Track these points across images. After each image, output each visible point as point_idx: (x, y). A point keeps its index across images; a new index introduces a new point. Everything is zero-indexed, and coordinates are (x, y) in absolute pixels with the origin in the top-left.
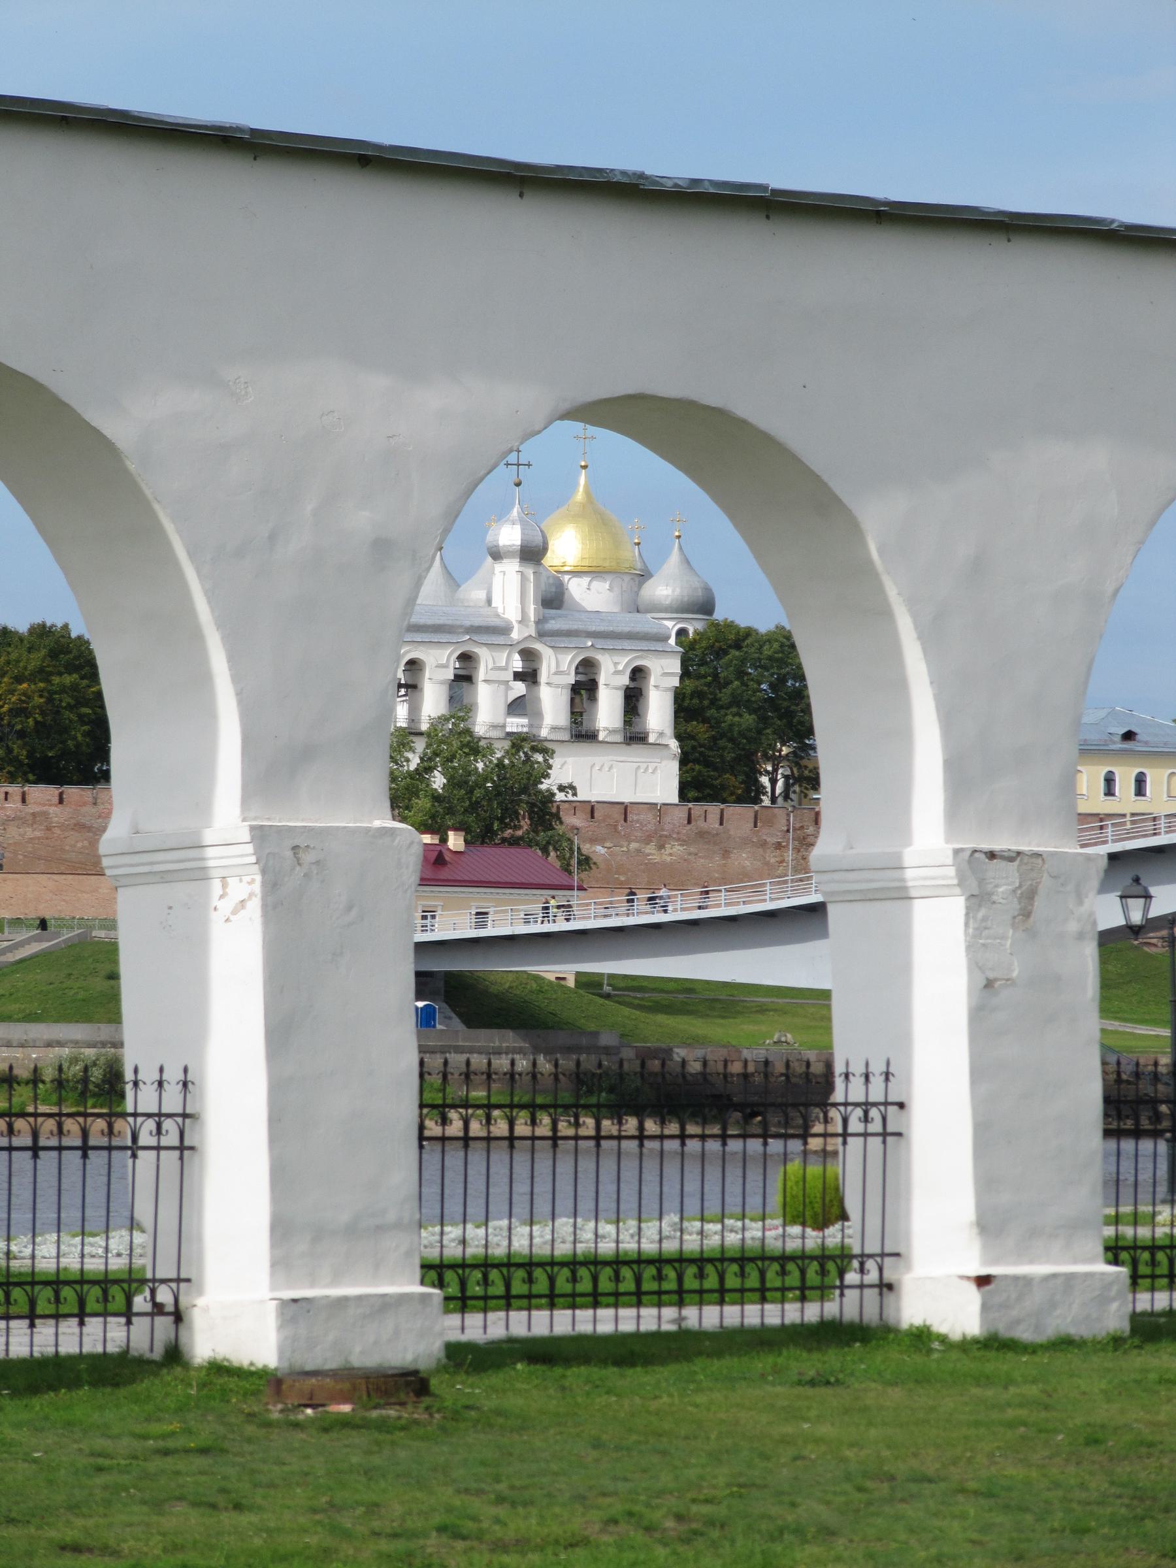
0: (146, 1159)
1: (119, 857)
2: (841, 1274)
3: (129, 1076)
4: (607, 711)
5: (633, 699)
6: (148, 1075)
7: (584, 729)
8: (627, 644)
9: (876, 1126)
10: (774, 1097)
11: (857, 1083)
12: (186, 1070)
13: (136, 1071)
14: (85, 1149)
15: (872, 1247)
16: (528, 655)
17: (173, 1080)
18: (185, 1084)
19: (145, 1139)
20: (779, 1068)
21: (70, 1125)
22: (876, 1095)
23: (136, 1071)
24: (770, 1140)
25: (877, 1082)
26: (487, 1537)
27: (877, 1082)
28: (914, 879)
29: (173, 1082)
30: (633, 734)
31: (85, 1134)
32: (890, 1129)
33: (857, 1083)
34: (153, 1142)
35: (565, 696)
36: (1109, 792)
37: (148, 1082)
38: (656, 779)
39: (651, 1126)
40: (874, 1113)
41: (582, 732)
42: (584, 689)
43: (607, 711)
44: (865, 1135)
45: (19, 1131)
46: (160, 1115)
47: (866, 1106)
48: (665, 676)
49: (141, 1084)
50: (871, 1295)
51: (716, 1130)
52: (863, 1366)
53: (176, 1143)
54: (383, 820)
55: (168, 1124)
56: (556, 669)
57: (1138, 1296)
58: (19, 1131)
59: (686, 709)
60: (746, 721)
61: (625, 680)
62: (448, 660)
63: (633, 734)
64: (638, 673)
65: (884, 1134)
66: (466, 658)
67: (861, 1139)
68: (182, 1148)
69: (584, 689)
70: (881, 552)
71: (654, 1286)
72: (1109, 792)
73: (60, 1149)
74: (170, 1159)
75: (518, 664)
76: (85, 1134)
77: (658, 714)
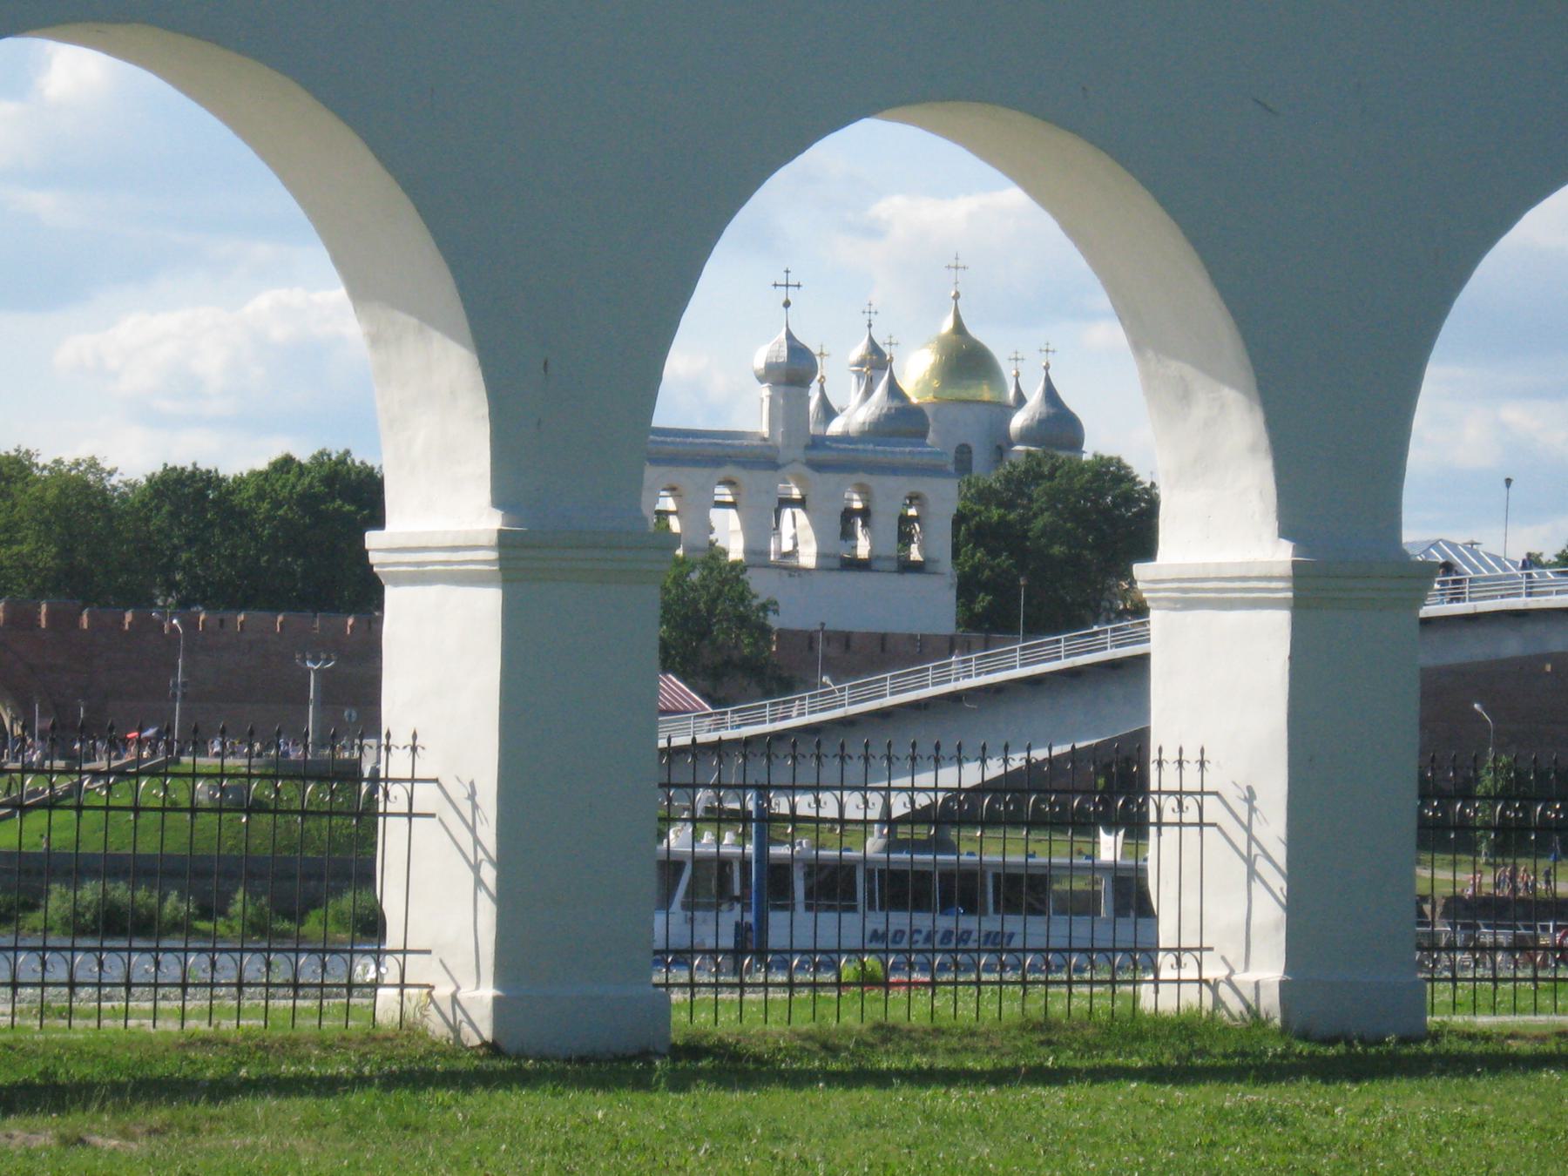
0: (1170, 834)
3: (1154, 755)
6: (1170, 755)
9: (1191, 815)
11: (1170, 770)
15: (1190, 941)
19: (1168, 816)
22: (1191, 783)
25: (1191, 770)
26: (120, 1127)
27: (1191, 770)
28: (1282, 590)
33: (1170, 770)
40: (1188, 801)
44: (1180, 824)
46: (1181, 793)
52: (1534, 1121)
55: (1188, 801)
67: (1177, 829)
70: (48, 614)
73: (1180, 824)
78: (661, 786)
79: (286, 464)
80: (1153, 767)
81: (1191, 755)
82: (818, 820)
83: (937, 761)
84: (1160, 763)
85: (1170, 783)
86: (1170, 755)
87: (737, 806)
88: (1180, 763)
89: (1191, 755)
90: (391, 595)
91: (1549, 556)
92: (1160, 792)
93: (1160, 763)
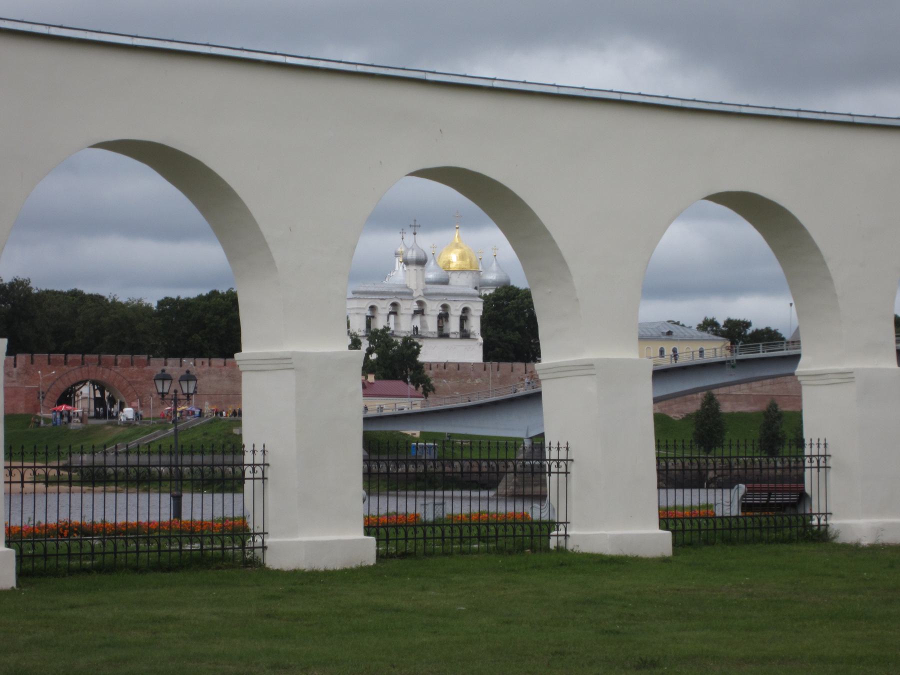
0: (554, 476)
2: (549, 532)
3: (547, 444)
4: (454, 325)
5: (464, 319)
6: (554, 445)
7: (445, 332)
8: (460, 299)
10: (527, 468)
14: (818, 467)
16: (420, 303)
19: (554, 469)
27: (815, 447)
30: (465, 335)
34: (251, 476)
35: (436, 320)
36: (675, 350)
38: (471, 352)
41: (443, 335)
42: (443, 317)
43: (454, 325)
48: (477, 309)
50: (562, 539)
51: (96, 470)
53: (20, 480)
54: (360, 535)
56: (433, 309)
57: (521, 511)
59: (486, 322)
60: (510, 326)
61: (460, 313)
63: (465, 335)
64: (465, 310)
66: (445, 307)
68: (264, 478)
69: (443, 317)
72: (675, 350)
74: (258, 483)
75: (415, 307)
77: (475, 325)
78: (268, 465)
79: (214, 293)
80: (547, 450)
81: (259, 448)
82: (379, 474)
83: (35, 454)
84: (550, 449)
85: (554, 456)
86: (554, 445)
87: (61, 472)
88: (254, 452)
89: (259, 448)
90: (244, 376)
91: (364, 378)
92: (550, 460)
93: (550, 449)
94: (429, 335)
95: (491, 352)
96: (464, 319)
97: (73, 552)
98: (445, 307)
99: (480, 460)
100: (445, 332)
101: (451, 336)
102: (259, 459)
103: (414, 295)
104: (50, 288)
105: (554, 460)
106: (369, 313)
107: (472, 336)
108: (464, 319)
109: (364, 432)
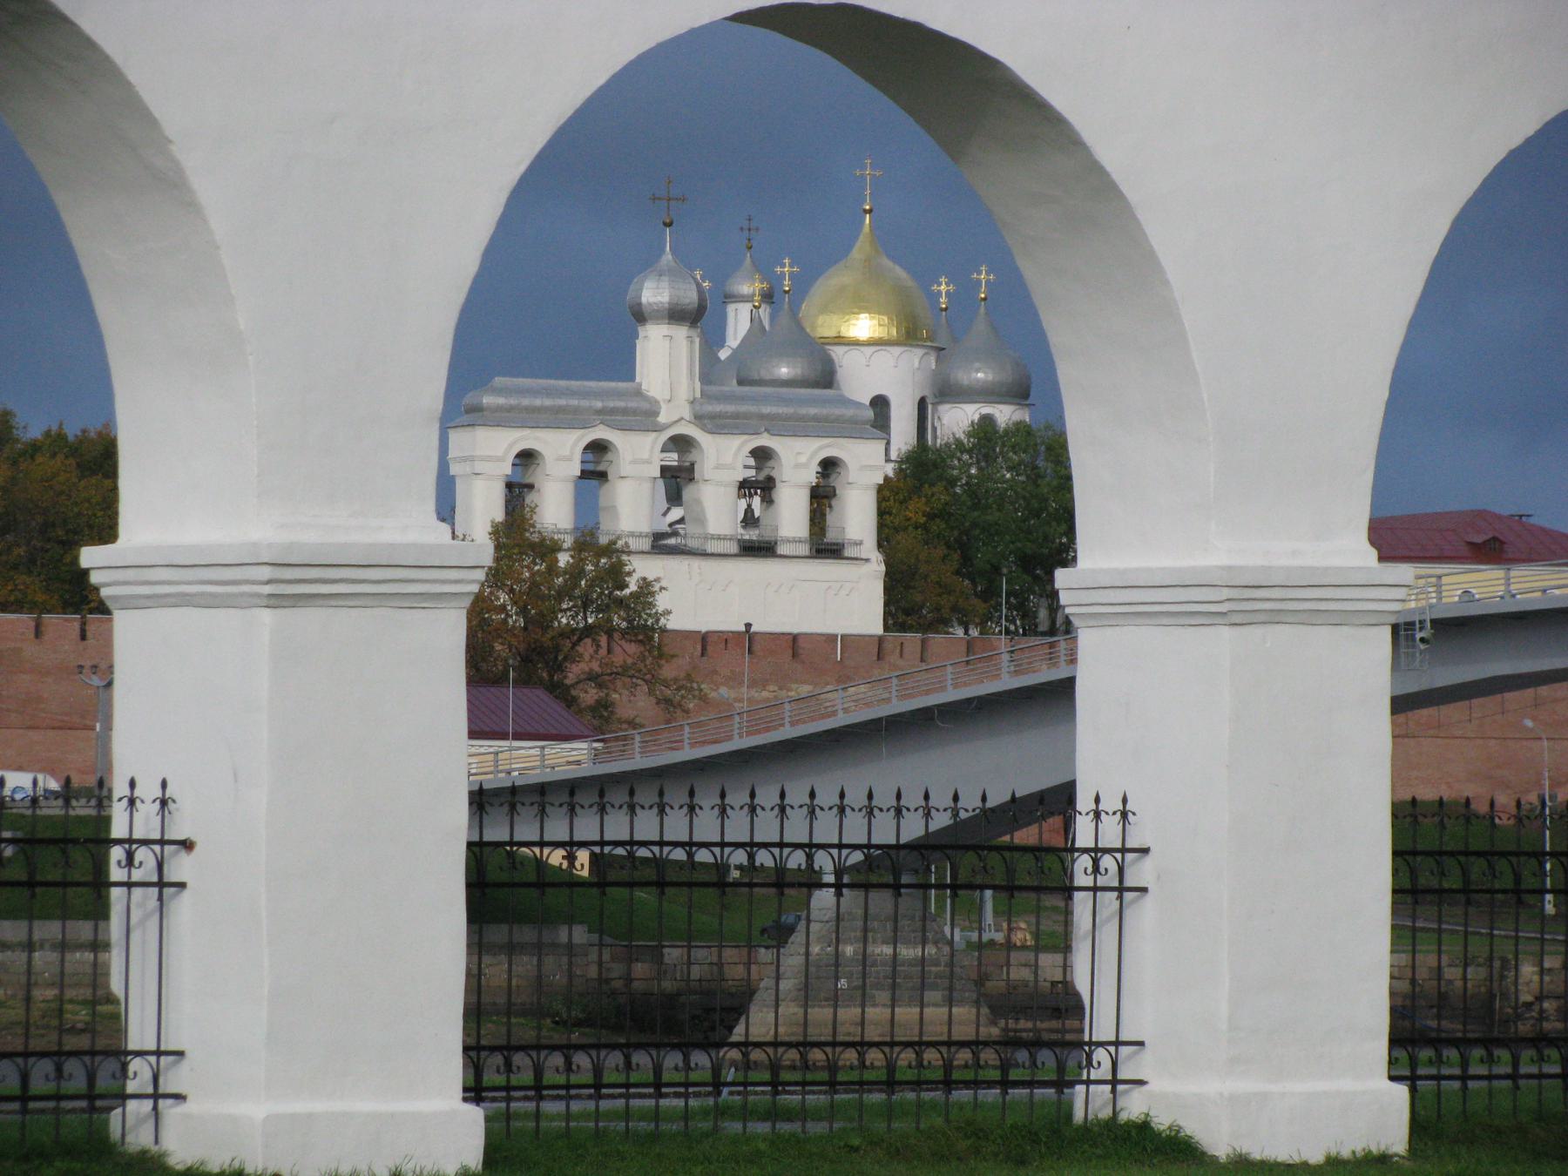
1: (239, 577)
7: (831, 536)
12: (164, 785)
13: (132, 784)
17: (149, 797)
18: (164, 803)
20: (1483, 808)
21: (582, 1060)
23: (132, 784)
24: (845, 891)
29: (149, 799)
30: (825, 546)
31: (538, 1072)
32: (1128, 883)
37: (768, 807)
39: (556, 858)
43: (790, 516)
45: (70, 1075)
47: (1096, 852)
49: (138, 802)
58: (70, 1075)
62: (736, 454)
65: (1121, 890)
66: (762, 455)
71: (500, 1080)
76: (538, 1072)
77: (857, 517)
81: (1111, 803)
89: (1111, 803)
94: (712, 547)
95: (906, 604)
96: (821, 498)
97: (899, 1076)
98: (762, 455)
99: (26, 1055)
100: (831, 536)
101: (782, 549)
102: (1110, 834)
103: (662, 418)
104: (458, 297)
105: (493, 1049)
106: (672, 459)
107: (847, 552)
108: (821, 498)
109: (477, 851)
